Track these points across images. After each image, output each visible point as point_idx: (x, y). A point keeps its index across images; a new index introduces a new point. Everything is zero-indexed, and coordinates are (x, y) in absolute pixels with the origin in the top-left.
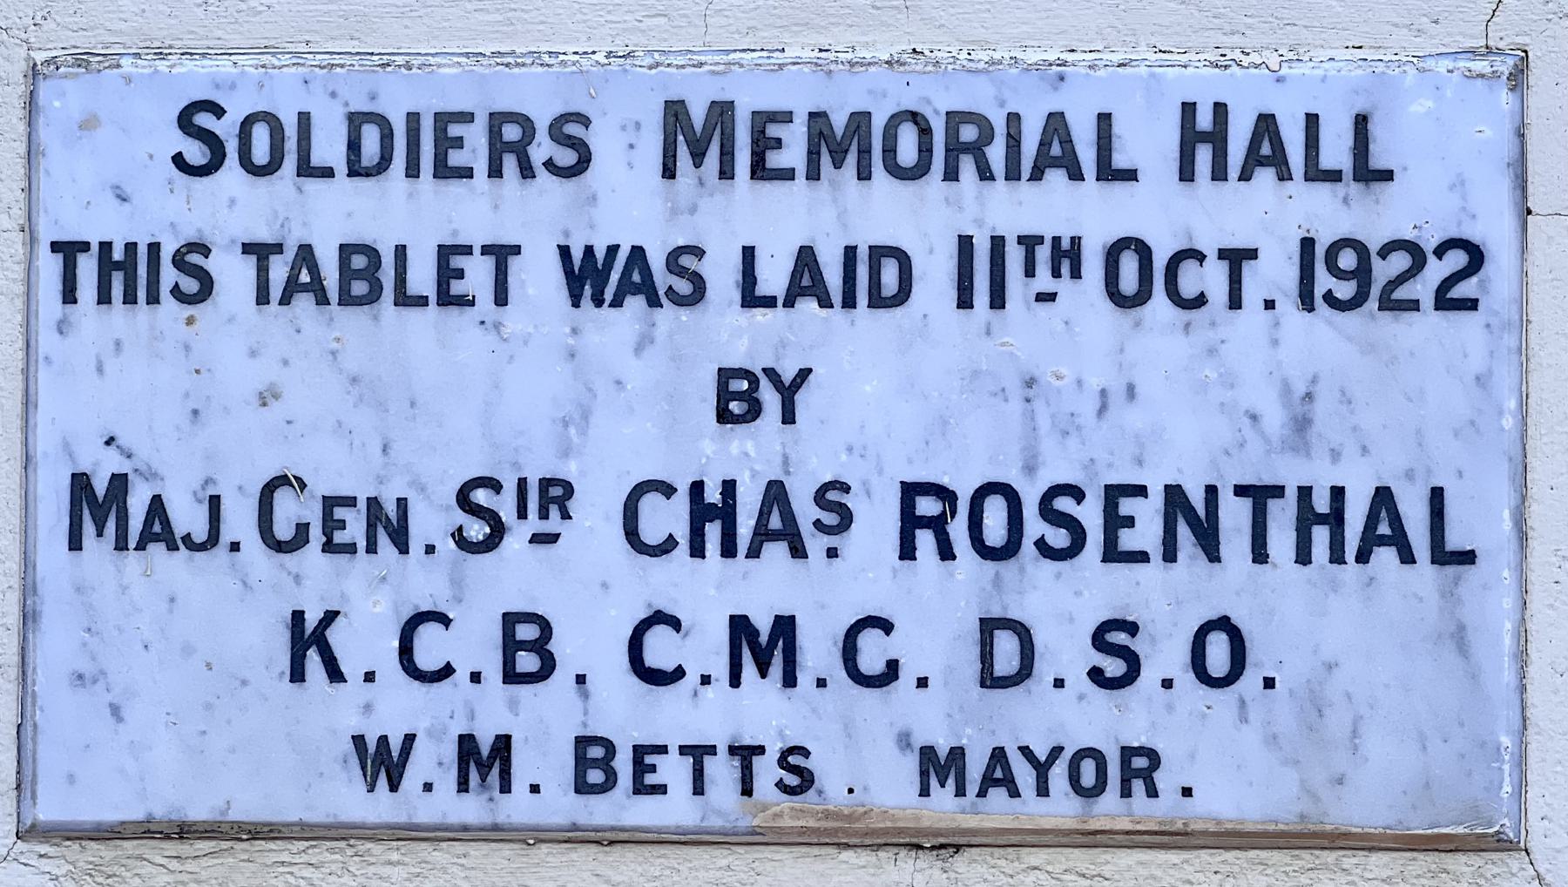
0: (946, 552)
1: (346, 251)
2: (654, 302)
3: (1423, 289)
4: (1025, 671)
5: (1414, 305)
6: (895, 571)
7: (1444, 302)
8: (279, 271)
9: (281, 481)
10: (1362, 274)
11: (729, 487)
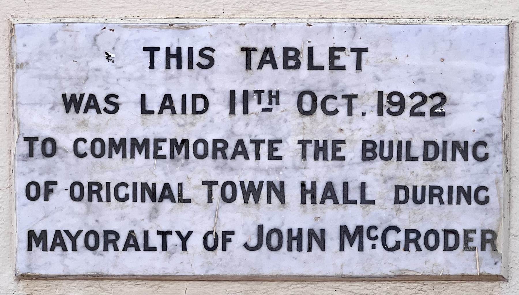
0: (419, 249)
1: (286, 50)
2: (99, 112)
3: (426, 108)
4: (205, 238)
5: (422, 114)
6: (162, 181)
7: (433, 114)
8: (256, 58)
9: (77, 141)
10: (402, 103)
11: (314, 184)
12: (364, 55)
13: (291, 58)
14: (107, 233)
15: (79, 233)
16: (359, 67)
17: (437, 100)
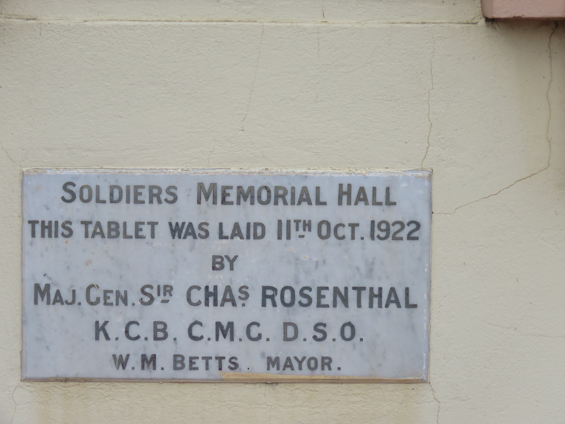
1: (110, 223)
2: (195, 237)
3: (404, 234)
5: (401, 239)
7: (410, 238)
8: (91, 229)
10: (388, 230)
12: (156, 227)
13: (113, 230)
14: (323, 358)
15: (304, 358)
16: (153, 236)
17: (413, 226)
